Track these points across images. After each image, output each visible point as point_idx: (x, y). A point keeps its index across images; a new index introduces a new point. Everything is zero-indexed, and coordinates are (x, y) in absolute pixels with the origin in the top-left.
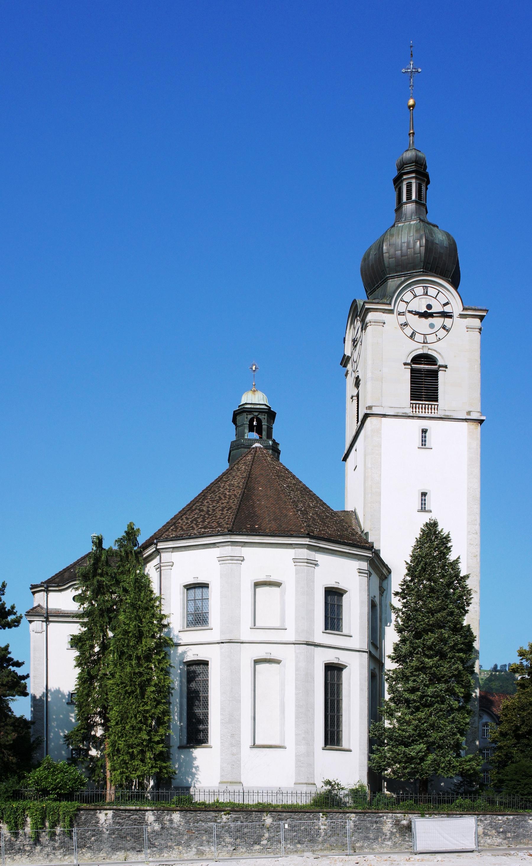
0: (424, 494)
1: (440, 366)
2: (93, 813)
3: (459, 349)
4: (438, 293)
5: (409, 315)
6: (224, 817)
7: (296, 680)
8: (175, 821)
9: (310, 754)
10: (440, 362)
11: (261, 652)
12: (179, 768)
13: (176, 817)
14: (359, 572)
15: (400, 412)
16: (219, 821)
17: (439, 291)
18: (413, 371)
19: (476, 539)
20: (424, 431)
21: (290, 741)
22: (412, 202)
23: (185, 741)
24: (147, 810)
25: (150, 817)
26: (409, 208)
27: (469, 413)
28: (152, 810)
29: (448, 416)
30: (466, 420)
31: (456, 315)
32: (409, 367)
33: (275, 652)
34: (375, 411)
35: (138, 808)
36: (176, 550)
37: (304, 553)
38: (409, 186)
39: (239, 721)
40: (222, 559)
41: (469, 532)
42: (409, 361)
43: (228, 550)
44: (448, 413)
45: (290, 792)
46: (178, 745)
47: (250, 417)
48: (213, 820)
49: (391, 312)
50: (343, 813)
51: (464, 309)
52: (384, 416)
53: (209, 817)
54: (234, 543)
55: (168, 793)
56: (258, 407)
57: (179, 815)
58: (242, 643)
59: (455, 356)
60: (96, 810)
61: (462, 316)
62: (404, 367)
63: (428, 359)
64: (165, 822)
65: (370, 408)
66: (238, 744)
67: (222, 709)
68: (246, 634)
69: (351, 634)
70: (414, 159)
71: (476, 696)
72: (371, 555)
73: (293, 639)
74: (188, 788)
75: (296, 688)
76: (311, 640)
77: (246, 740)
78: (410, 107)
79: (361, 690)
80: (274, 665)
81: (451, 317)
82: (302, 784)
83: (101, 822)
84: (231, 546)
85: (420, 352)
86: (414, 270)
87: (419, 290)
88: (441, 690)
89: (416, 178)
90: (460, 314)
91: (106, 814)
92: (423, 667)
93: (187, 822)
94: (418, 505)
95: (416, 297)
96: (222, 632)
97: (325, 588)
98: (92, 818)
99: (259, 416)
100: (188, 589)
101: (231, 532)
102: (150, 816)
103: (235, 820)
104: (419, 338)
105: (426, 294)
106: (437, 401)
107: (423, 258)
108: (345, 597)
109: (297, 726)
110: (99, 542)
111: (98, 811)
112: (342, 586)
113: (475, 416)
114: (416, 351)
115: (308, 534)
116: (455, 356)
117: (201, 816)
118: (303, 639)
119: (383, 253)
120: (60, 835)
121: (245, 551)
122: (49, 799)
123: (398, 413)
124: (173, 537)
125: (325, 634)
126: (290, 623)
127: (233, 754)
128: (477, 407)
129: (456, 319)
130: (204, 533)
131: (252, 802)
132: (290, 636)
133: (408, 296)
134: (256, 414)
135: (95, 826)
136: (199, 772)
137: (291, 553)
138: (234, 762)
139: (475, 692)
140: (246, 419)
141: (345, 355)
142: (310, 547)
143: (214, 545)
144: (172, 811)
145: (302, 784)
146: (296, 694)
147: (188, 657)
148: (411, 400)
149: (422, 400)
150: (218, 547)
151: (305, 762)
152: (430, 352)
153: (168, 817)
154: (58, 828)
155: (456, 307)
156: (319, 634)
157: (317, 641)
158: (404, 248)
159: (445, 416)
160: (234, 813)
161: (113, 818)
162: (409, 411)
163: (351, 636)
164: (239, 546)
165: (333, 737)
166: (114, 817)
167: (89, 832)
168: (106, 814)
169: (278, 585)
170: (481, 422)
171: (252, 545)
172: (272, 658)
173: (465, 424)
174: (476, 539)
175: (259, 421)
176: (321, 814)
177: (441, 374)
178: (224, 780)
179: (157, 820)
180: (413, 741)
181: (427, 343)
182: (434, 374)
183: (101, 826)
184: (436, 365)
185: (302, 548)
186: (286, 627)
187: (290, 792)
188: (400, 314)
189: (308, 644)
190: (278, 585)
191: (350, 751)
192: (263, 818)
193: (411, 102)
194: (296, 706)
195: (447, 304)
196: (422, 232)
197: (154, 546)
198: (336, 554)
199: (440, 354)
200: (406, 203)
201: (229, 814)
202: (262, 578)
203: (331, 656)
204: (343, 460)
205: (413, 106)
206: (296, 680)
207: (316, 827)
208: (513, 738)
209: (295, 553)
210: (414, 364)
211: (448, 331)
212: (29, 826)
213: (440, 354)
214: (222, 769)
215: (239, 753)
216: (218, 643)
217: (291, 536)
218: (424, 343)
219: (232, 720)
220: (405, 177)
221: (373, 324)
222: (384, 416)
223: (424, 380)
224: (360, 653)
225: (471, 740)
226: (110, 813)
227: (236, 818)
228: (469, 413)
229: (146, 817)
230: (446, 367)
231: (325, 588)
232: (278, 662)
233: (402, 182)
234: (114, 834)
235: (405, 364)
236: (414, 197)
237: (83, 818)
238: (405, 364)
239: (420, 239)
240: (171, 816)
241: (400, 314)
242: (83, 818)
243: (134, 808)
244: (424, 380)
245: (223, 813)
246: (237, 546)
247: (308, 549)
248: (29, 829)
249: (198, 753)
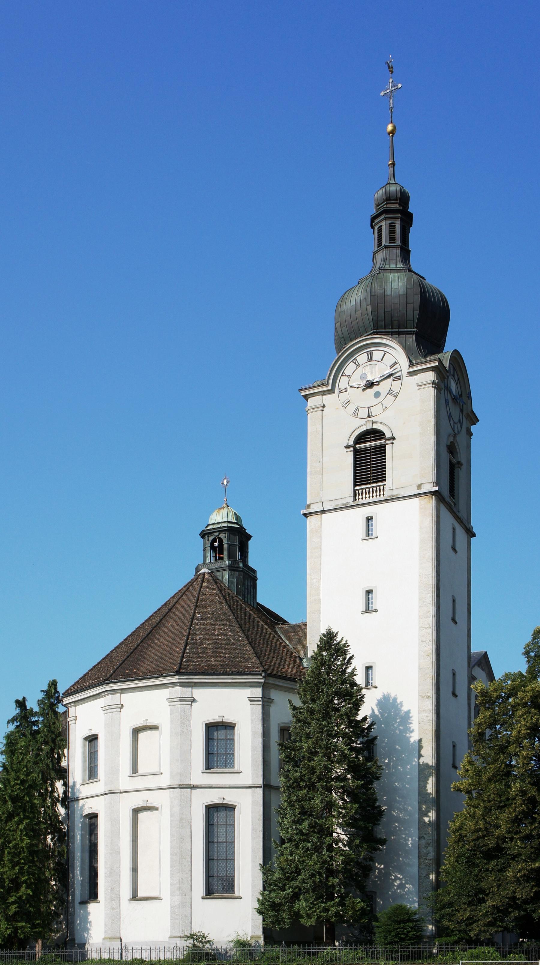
4: (385, 354)
7: (171, 827)
10: (388, 435)
11: (138, 800)
12: (80, 924)
14: (250, 701)
18: (356, 452)
19: (429, 634)
20: (369, 519)
21: (166, 894)
23: (87, 896)
27: (419, 487)
29: (394, 496)
30: (416, 496)
32: (352, 449)
33: (153, 799)
37: (178, 691)
39: (119, 874)
41: (421, 627)
42: (351, 443)
44: (395, 493)
46: (79, 901)
47: (211, 538)
52: (323, 512)
54: (112, 691)
55: (24, 953)
58: (121, 793)
59: (404, 423)
61: (411, 374)
62: (346, 450)
63: (374, 434)
67: (106, 862)
71: (430, 821)
72: (263, 681)
74: (84, 945)
76: (187, 782)
77: (126, 892)
79: (254, 830)
81: (399, 378)
82: (176, 937)
84: (112, 694)
85: (364, 428)
90: (408, 373)
96: (106, 784)
99: (220, 536)
106: (385, 480)
107: (371, 319)
109: (172, 875)
110: (21, 704)
112: (228, 719)
114: (358, 430)
116: (404, 423)
118: (177, 782)
121: (126, 698)
123: (337, 505)
125: (205, 774)
127: (113, 909)
129: (406, 379)
131: (127, 958)
132: (165, 781)
134: (217, 534)
136: (92, 928)
137: (166, 693)
139: (428, 816)
140: (207, 542)
142: (182, 684)
145: (176, 937)
146: (171, 842)
147: (86, 811)
149: (370, 484)
152: (375, 426)
156: (199, 776)
157: (194, 782)
159: (390, 496)
163: (241, 772)
164: (118, 693)
165: (219, 883)
171: (130, 691)
173: (416, 500)
174: (429, 634)
175: (221, 541)
182: (382, 450)
185: (175, 686)
189: (181, 787)
194: (171, 854)
195: (396, 363)
198: (219, 686)
202: (139, 723)
203: (214, 797)
211: (396, 396)
216: (102, 795)
221: (312, 411)
222: (323, 512)
223: (369, 458)
224: (252, 789)
225: (424, 875)
228: (419, 487)
235: (347, 447)
238: (347, 447)
244: (369, 458)
246: (116, 693)
247: (181, 686)
249: (92, 907)
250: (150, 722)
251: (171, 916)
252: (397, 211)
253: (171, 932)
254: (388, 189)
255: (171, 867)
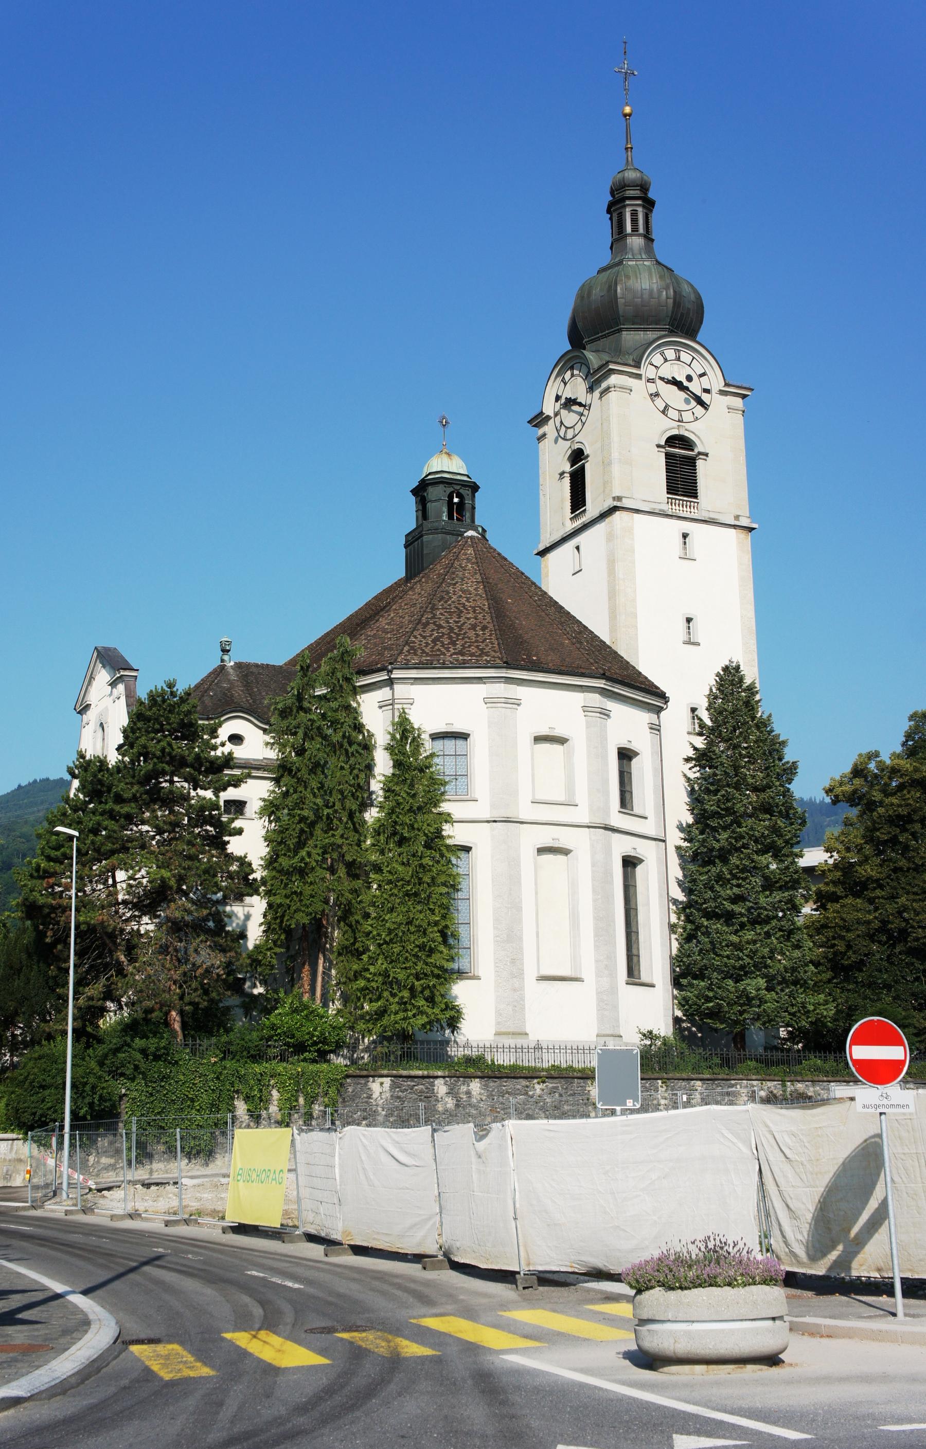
0: (689, 620)
1: (700, 453)
2: (363, 1082)
3: (720, 432)
5: (659, 382)
6: (537, 1086)
8: (474, 1093)
9: (613, 990)
10: (700, 448)
11: (546, 836)
13: (475, 1086)
14: (651, 728)
15: (657, 508)
16: (531, 1093)
17: (694, 358)
18: (668, 456)
20: (685, 536)
21: (588, 971)
22: (639, 235)
24: (437, 1077)
25: (441, 1087)
26: (636, 242)
27: (737, 517)
28: (444, 1077)
31: (715, 390)
33: (564, 838)
34: (626, 503)
35: (426, 1073)
36: (418, 681)
37: (595, 699)
38: (634, 214)
39: (521, 939)
40: (488, 701)
42: (663, 443)
43: (500, 689)
44: (713, 516)
45: (488, 1045)
48: (524, 1092)
49: (639, 377)
50: (687, 1080)
51: (726, 385)
52: (637, 511)
53: (519, 1087)
54: (509, 680)
56: (459, 477)
57: (479, 1085)
60: (367, 1076)
61: (722, 393)
62: (657, 449)
64: (461, 1096)
65: (619, 499)
66: (520, 975)
68: (526, 812)
69: (647, 815)
70: (639, 183)
73: (586, 821)
75: (594, 891)
78: (625, 115)
80: (561, 858)
83: (374, 1096)
85: (675, 432)
86: (656, 324)
87: (670, 353)
88: (780, 901)
89: (644, 207)
90: (720, 390)
91: (382, 1084)
92: (755, 868)
93: (490, 1096)
94: (681, 634)
95: (668, 361)
97: (619, 749)
98: (362, 1090)
100: (433, 739)
101: (509, 665)
102: (441, 1087)
103: (552, 1092)
104: (672, 413)
105: (678, 359)
106: (696, 497)
108: (634, 761)
111: (371, 1079)
113: (745, 522)
115: (604, 674)
117: (508, 1085)
118: (599, 820)
119: (616, 298)
120: (318, 1118)
122: (305, 1060)
124: (416, 664)
126: (582, 796)
127: (515, 990)
128: (745, 511)
130: (464, 662)
132: (582, 815)
133: (657, 359)
134: (458, 487)
135: (366, 1102)
137: (579, 698)
138: (515, 1002)
141: (542, 413)
142: (603, 692)
143: (480, 680)
144: (470, 1077)
148: (668, 493)
150: (485, 683)
151: (607, 1004)
152: (686, 434)
153: (464, 1088)
154: (317, 1107)
155: (715, 380)
158: (646, 296)
160: (550, 1080)
161: (390, 1091)
162: (667, 508)
163: (646, 818)
166: (393, 1087)
167: (359, 1113)
168: (382, 1084)
169: (562, 741)
170: (751, 529)
171: (532, 684)
172: (561, 846)
173: (733, 531)
176: (660, 1082)
177: (700, 463)
178: (503, 1030)
179: (451, 1092)
180: (746, 974)
181: (682, 421)
182: (691, 462)
183: (374, 1103)
184: (693, 450)
186: (577, 802)
187: (488, 1045)
188: (649, 380)
190: (562, 741)
191: (653, 986)
192: (588, 1089)
193: (627, 110)
194: (595, 918)
196: (668, 281)
197: (385, 673)
199: (699, 437)
200: (631, 235)
201: (544, 1082)
202: (544, 731)
204: (537, 554)
205: (630, 115)
206: (593, 879)
207: (655, 1102)
208: (828, 969)
209: (585, 700)
210: (670, 446)
212: (276, 1103)
213: (699, 437)
214: (499, 1013)
215: (522, 988)
216: (488, 822)
217: (583, 675)
218: (679, 421)
219: (510, 937)
220: (628, 202)
222: (637, 511)
223: (681, 470)
226: (387, 1081)
227: (554, 1088)
229: (436, 1088)
230: (707, 455)
231: (619, 749)
232: (565, 852)
233: (625, 206)
234: (392, 1115)
235: (658, 446)
236: (641, 230)
237: (350, 1090)
239: (667, 288)
240: (468, 1086)
241: (649, 380)
242: (350, 1090)
243: (420, 1073)
244: (681, 470)
245: (536, 1081)
248: (276, 1109)
250: (558, 732)
251: (598, 1005)
252: (628, 200)
253: (598, 1028)
254: (626, 175)
255: (596, 935)
